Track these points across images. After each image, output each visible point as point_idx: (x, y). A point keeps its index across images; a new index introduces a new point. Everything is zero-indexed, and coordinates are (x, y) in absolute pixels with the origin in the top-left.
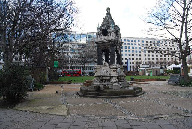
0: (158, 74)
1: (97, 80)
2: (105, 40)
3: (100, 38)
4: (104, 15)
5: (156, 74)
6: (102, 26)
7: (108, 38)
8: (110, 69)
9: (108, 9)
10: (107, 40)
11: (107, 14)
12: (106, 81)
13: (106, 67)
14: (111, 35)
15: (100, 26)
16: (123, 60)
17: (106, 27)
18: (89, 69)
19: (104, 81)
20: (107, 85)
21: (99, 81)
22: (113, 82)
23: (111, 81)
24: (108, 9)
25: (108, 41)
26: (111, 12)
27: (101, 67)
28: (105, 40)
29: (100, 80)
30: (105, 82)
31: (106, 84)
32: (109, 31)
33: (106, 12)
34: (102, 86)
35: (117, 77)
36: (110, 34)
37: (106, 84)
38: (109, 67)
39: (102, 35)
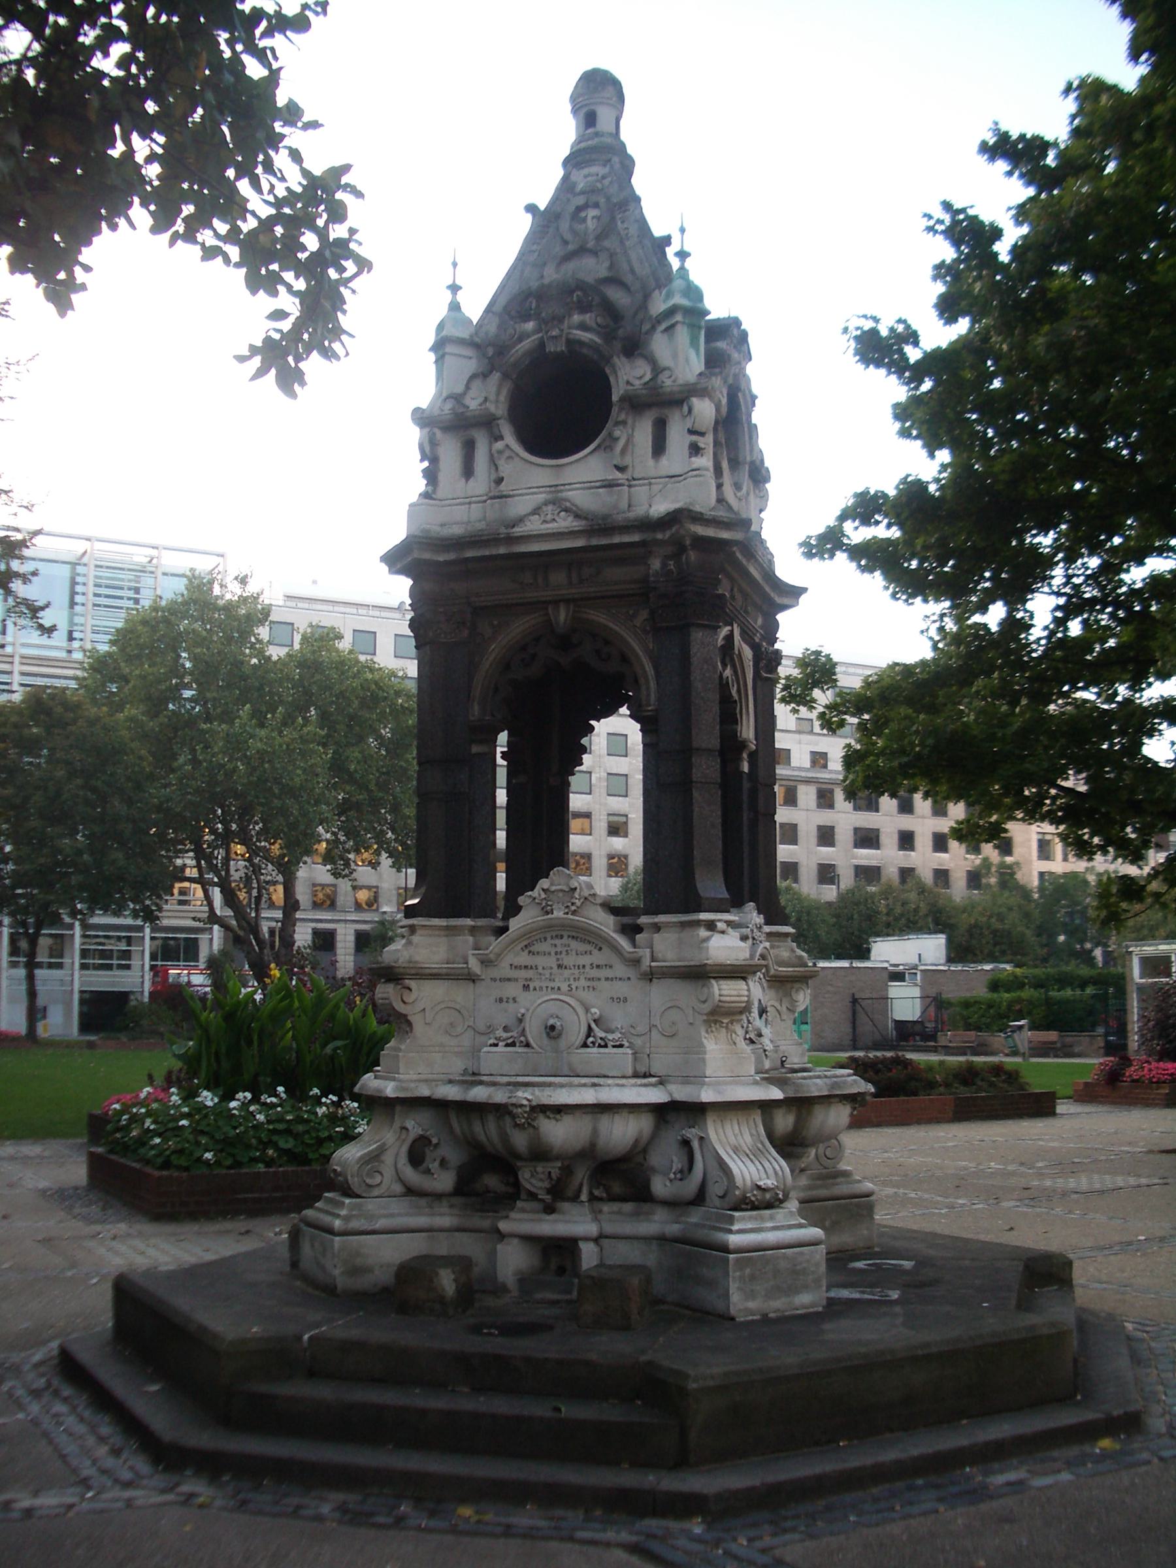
0: (865, 1027)
1: (416, 1157)
2: (909, 523)
3: (480, 484)
4: (535, 164)
5: (847, 1028)
6: (522, 299)
7: (610, 485)
8: (650, 976)
9: (598, 95)
10: (599, 525)
11: (573, 161)
12: (581, 1174)
13: (578, 956)
14: (659, 448)
15: (474, 308)
16: (791, 799)
17: (582, 329)
18: (84, 953)
19: (533, 1179)
20: (589, 1256)
21: (444, 1181)
22: (700, 1198)
23: (660, 1186)
24: (598, 95)
25: (626, 528)
26: (634, 132)
27: (495, 945)
28: (565, 522)
29: (455, 1156)
30: (558, 1195)
31: (574, 1222)
32: (628, 376)
33: (564, 133)
34: (512, 1261)
35: (766, 1106)
36: (643, 433)
37: (574, 1222)
38: (623, 942)
39: (510, 439)
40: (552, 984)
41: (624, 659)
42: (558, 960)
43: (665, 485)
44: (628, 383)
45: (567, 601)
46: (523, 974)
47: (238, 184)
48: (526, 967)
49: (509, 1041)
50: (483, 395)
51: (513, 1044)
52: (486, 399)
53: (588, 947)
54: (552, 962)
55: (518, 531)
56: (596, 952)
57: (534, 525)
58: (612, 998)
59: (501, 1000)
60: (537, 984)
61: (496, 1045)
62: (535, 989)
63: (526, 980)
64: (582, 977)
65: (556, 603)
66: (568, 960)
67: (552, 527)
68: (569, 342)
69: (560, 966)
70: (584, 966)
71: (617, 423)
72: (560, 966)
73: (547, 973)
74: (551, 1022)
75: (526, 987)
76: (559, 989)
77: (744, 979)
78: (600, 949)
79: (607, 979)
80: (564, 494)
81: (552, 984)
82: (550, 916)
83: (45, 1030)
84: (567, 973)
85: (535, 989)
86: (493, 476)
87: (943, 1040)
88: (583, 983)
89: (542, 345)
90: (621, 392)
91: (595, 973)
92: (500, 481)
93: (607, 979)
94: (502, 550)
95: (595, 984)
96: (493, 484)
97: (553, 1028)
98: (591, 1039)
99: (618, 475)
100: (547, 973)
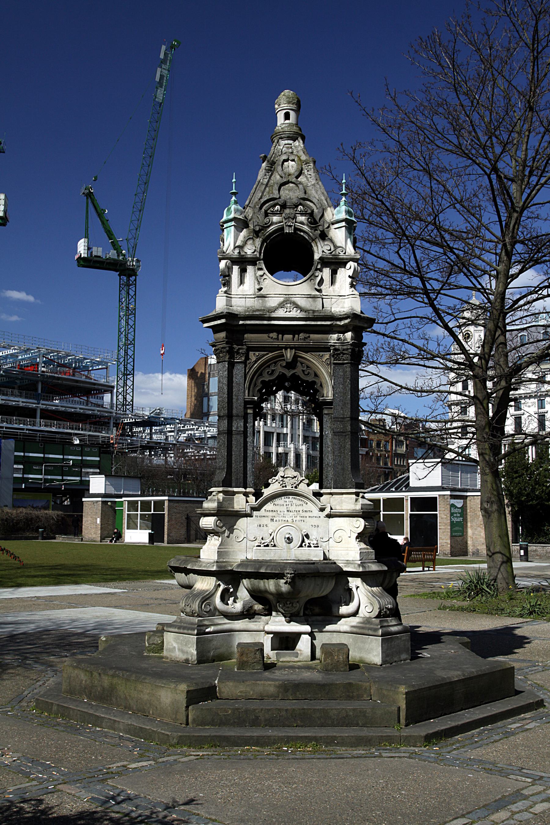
40: (284, 519)
41: (316, 375)
42: (287, 508)
43: (338, 299)
44: (323, 251)
45: (291, 348)
46: (271, 514)
47: (312, 243)
48: (272, 511)
49: (265, 544)
50: (254, 248)
51: (267, 546)
52: (255, 251)
53: (301, 503)
54: (284, 509)
55: (274, 315)
56: (304, 505)
57: (281, 313)
58: (312, 525)
59: (260, 526)
60: (277, 519)
61: (260, 546)
62: (276, 521)
63: (272, 517)
64: (298, 516)
65: (286, 348)
66: (292, 508)
67: (288, 315)
68: (296, 229)
69: (288, 511)
70: (299, 511)
71: (317, 269)
72: (288, 511)
73: (282, 513)
74: (287, 536)
75: (272, 520)
76: (287, 521)
77: (372, 518)
78: (307, 504)
79: (310, 517)
80: (293, 299)
81: (284, 519)
82: (285, 488)
83: (238, 505)
84: (291, 514)
85: (276, 521)
86: (257, 287)
87: (408, 569)
88: (298, 518)
89: (282, 229)
90: (320, 255)
91: (304, 514)
92: (260, 289)
93: (310, 517)
94: (265, 322)
95: (304, 519)
96: (256, 290)
97: (288, 538)
98: (304, 544)
99: (318, 293)
100: (282, 513)
